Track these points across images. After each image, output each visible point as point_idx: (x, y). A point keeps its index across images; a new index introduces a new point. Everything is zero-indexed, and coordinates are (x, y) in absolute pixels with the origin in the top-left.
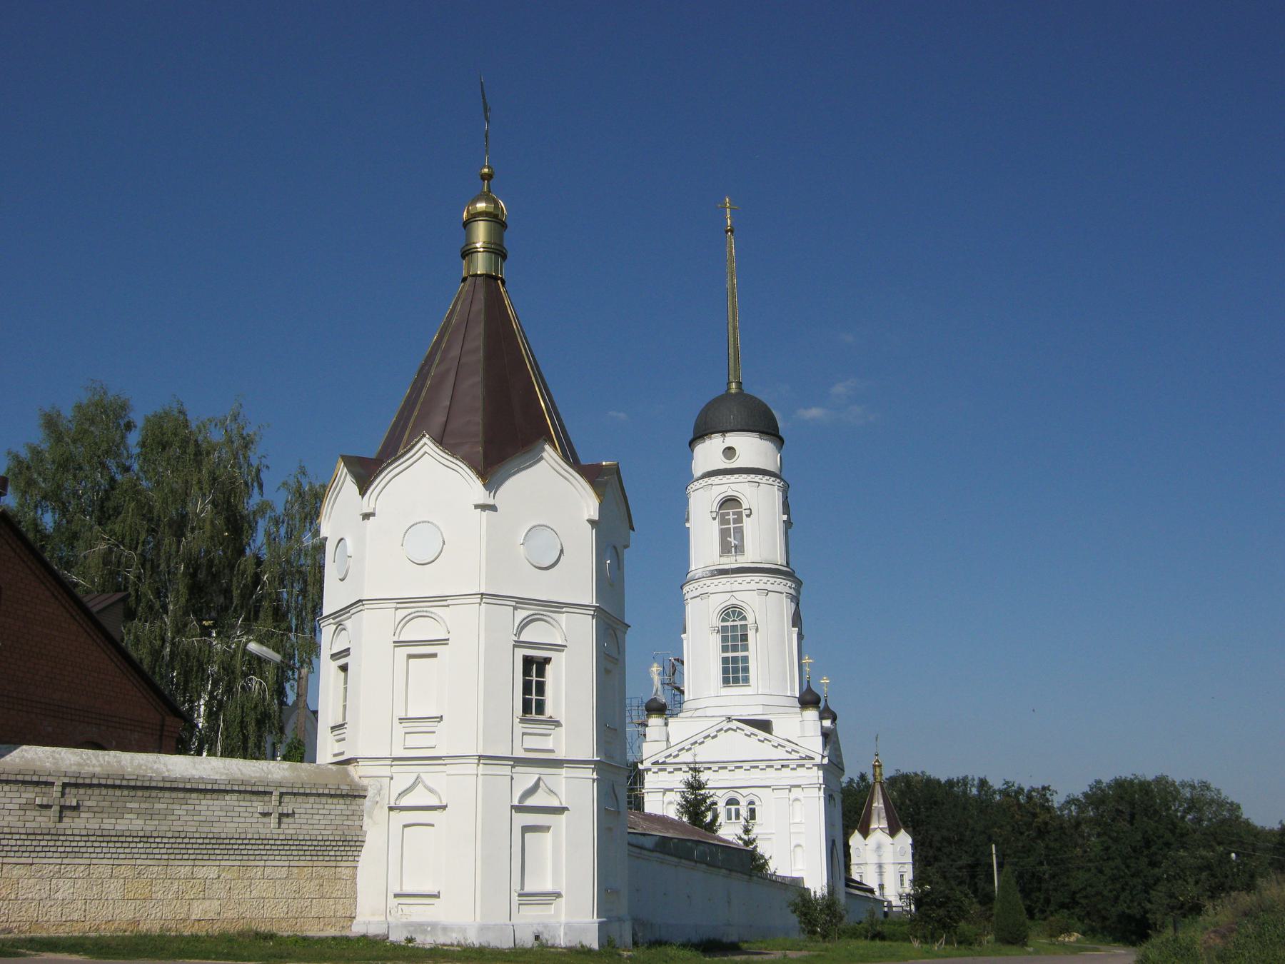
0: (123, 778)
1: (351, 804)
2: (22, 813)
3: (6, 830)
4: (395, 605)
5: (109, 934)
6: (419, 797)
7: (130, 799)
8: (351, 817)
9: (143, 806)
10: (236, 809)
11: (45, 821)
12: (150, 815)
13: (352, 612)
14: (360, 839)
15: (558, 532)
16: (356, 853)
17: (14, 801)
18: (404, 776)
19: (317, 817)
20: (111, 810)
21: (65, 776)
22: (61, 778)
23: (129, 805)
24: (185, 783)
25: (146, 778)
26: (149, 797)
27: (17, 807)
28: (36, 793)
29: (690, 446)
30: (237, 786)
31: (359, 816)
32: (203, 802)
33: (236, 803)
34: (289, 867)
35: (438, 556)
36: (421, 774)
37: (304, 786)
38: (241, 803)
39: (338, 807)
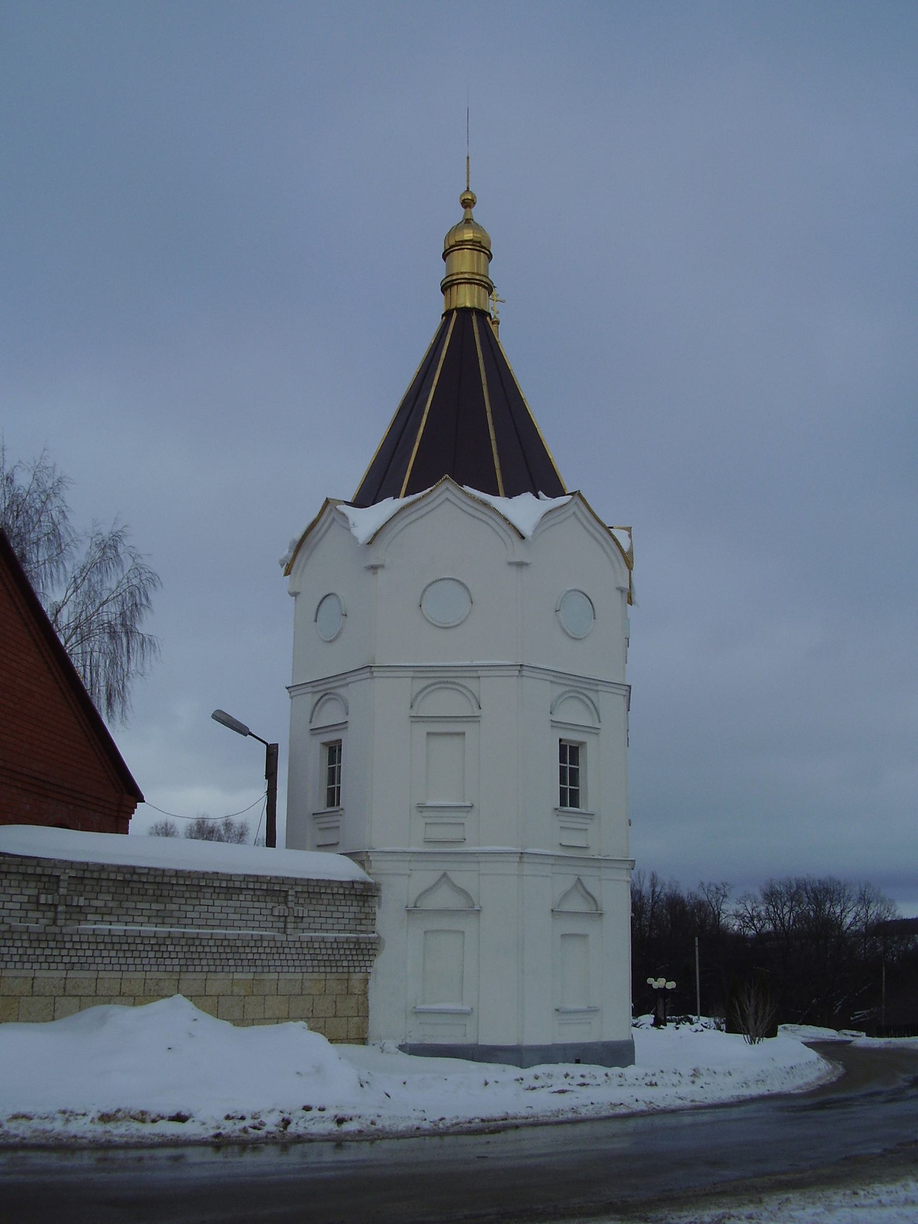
0: (135, 873)
1: (364, 906)
2: (23, 913)
3: (7, 935)
4: (412, 674)
5: (892, 1047)
6: (444, 898)
7: (140, 898)
8: (363, 922)
9: (155, 906)
10: (251, 911)
11: (37, 923)
12: (162, 918)
13: (348, 680)
14: (373, 947)
15: (594, 604)
16: (368, 964)
17: (15, 898)
18: (425, 877)
19: (330, 921)
20: (120, 911)
21: (72, 868)
22: (67, 871)
23: (140, 906)
24: (199, 879)
25: (158, 873)
26: (161, 896)
27: (18, 906)
28: (39, 889)
29: (539, 499)
30: (239, 883)
31: (372, 919)
32: (217, 903)
33: (250, 904)
34: (121, 979)
35: (319, 606)
36: (447, 872)
37: (233, 879)
38: (256, 904)
39: (352, 909)
